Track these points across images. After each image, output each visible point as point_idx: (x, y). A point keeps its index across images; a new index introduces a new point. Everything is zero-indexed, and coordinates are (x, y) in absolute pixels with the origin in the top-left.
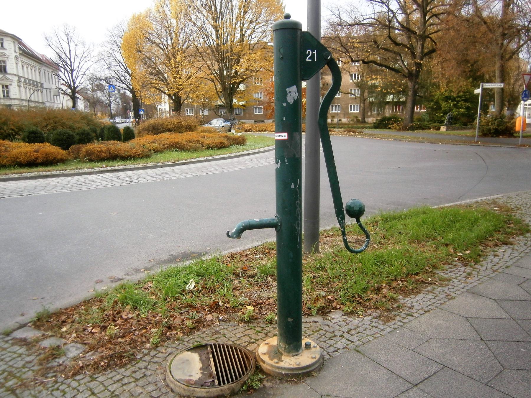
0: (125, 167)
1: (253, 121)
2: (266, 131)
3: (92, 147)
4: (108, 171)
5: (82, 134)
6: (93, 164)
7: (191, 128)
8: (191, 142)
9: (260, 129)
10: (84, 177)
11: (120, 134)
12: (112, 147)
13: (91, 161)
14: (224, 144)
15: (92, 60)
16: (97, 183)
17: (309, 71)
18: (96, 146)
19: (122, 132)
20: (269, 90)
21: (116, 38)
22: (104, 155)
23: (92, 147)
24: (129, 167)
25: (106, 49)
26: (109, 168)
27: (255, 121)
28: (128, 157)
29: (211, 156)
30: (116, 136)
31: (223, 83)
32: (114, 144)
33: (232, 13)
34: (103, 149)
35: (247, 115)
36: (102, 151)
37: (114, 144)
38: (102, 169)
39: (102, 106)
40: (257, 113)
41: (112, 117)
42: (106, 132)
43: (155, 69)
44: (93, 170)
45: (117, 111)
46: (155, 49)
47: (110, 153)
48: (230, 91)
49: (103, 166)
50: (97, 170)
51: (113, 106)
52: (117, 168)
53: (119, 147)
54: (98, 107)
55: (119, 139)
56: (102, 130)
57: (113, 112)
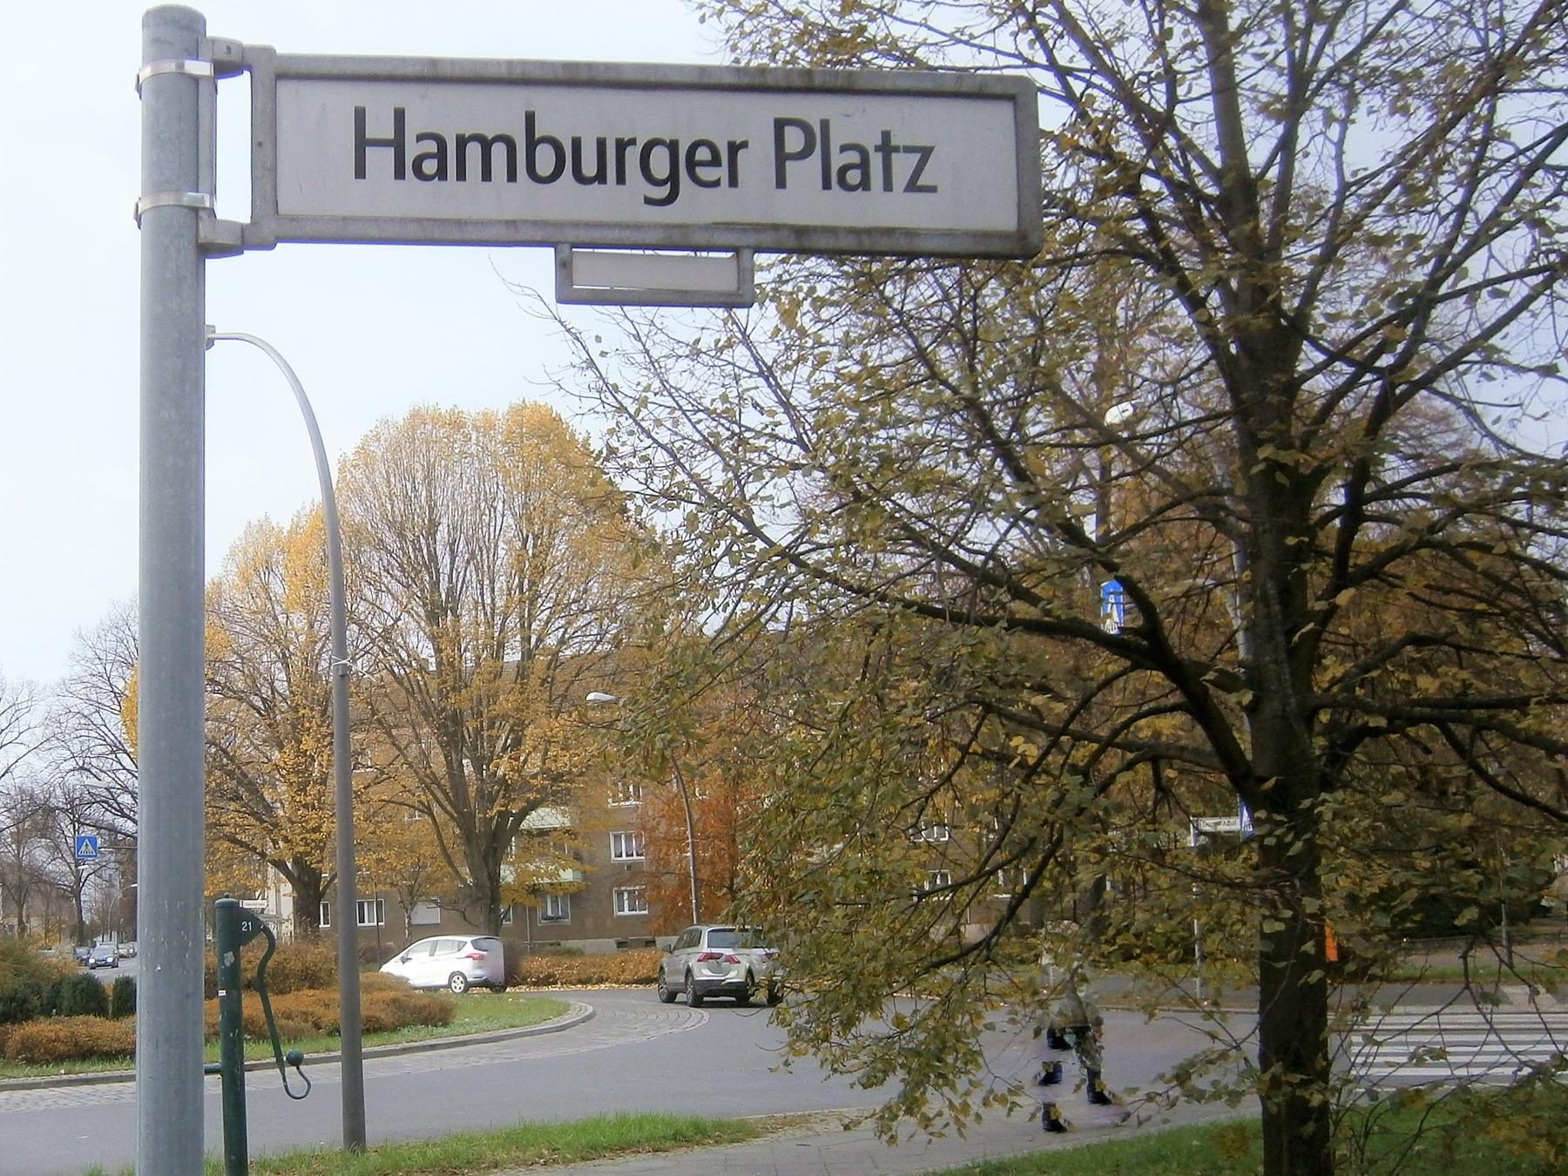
0: (108, 1074)
1: (612, 942)
2: (601, 980)
3: (35, 1029)
4: (70, 1083)
5: (12, 999)
6: (35, 1070)
7: (318, 979)
8: (289, 1017)
9: (584, 977)
10: (19, 1094)
11: (105, 999)
12: (82, 1029)
13: (31, 1061)
14: (378, 1020)
15: (23, 738)
16: (49, 1102)
17: (246, 938)
18: (43, 1028)
19: (110, 992)
20: (654, 829)
21: (108, 667)
22: (62, 1048)
23: (35, 1029)
24: (117, 1073)
25: (71, 701)
26: (73, 1076)
27: (620, 945)
28: (119, 1052)
29: (328, 1050)
30: (93, 1005)
31: (464, 820)
32: (86, 1023)
33: (492, 582)
34: (61, 1034)
35: (589, 923)
36: (58, 1039)
37: (86, 1023)
38: (57, 1078)
39: (46, 897)
40: (626, 912)
41: (83, 935)
42: (66, 993)
43: (230, 774)
44: (38, 1079)
45: (103, 914)
46: (236, 711)
47: (76, 1044)
48: (489, 844)
49: (61, 1073)
50: (48, 1079)
51: (89, 894)
52: (91, 1075)
53: (96, 1030)
54: (36, 903)
55: (101, 1011)
56: (57, 987)
57: (86, 917)
